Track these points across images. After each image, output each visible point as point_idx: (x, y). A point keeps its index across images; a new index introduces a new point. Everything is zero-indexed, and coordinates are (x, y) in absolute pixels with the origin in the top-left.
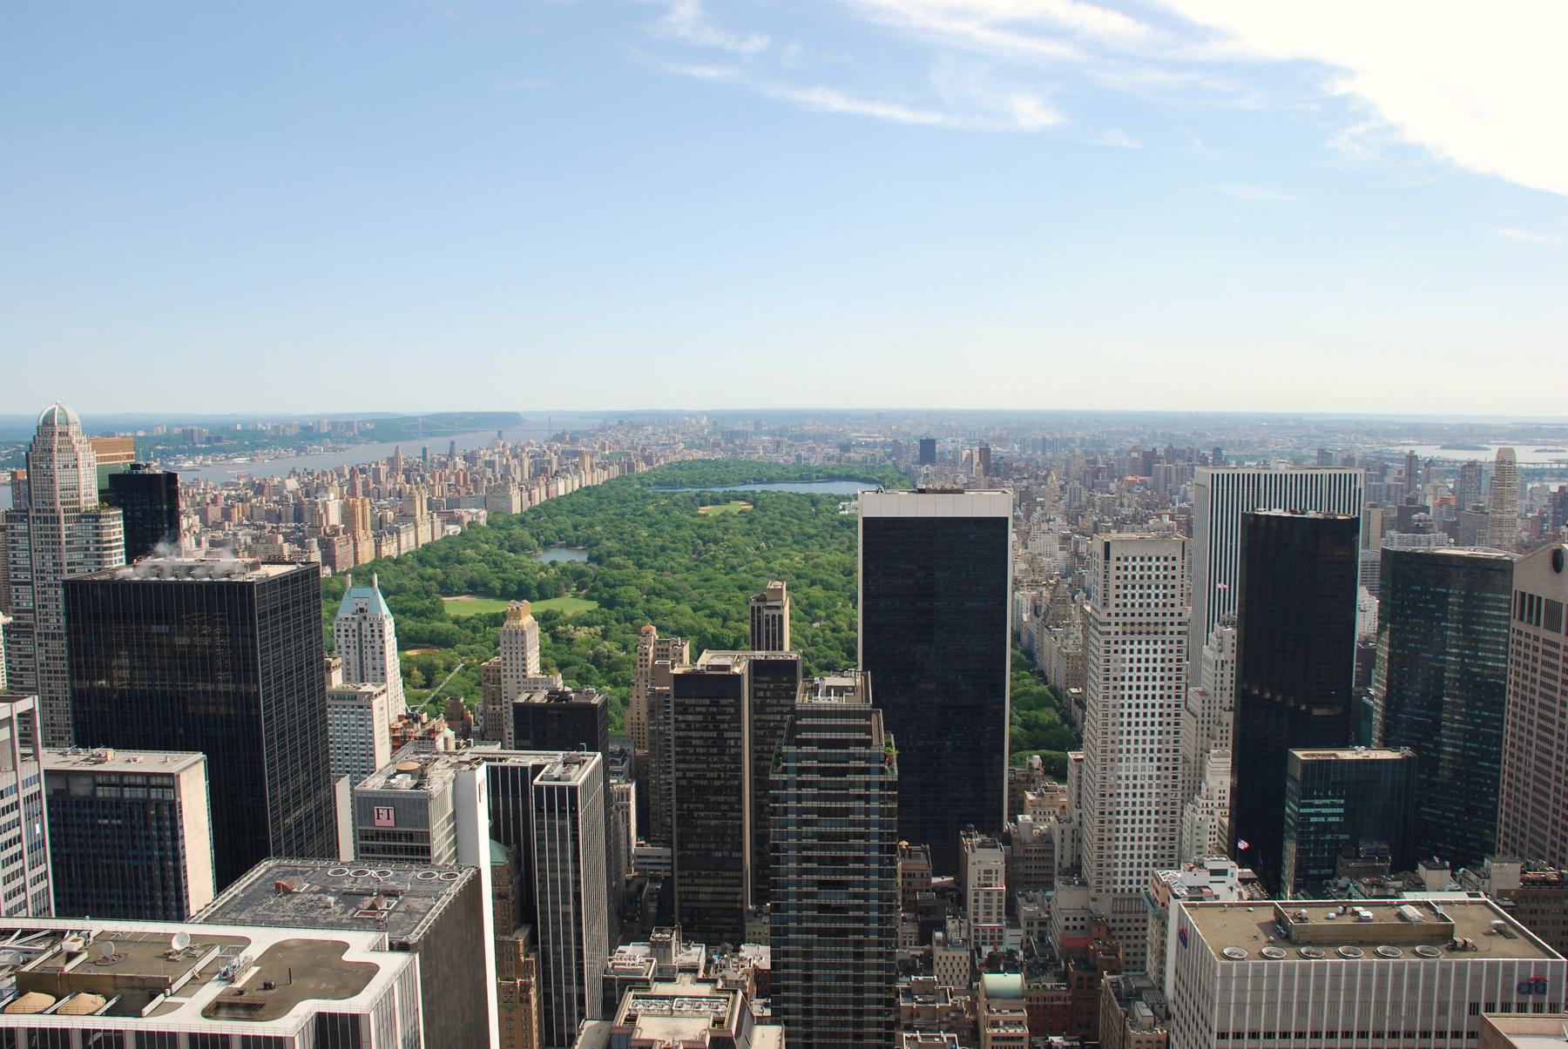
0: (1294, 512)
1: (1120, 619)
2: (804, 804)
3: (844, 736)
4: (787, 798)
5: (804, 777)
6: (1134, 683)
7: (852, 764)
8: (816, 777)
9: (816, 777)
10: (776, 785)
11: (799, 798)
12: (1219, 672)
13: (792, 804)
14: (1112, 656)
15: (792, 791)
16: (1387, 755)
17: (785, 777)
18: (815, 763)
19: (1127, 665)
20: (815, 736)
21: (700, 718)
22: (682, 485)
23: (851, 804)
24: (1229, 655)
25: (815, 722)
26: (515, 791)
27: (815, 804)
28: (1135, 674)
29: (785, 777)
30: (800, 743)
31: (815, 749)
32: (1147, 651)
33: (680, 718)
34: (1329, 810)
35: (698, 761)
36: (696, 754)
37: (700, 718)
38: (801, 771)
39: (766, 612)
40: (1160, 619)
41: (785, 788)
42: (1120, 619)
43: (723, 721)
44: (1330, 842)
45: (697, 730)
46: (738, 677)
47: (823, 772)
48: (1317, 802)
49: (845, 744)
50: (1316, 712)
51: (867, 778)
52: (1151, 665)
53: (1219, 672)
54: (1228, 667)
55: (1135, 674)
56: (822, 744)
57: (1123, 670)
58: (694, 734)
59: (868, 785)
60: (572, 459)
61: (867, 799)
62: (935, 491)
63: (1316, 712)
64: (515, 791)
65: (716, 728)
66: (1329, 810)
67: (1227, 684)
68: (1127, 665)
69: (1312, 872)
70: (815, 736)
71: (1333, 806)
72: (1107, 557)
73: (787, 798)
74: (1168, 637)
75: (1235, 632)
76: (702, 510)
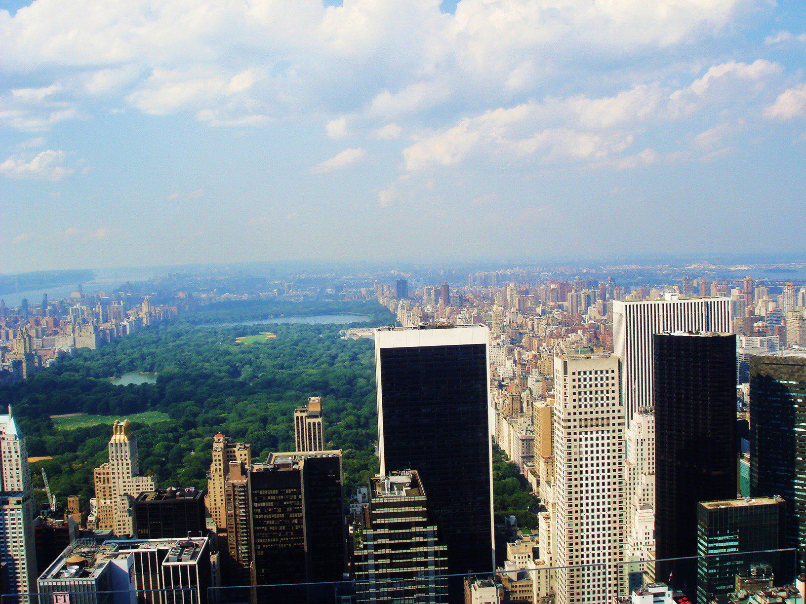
0: (691, 332)
1: (578, 417)
2: (381, 571)
3: (407, 520)
4: (367, 568)
5: (380, 552)
6: (589, 462)
7: (414, 540)
8: (388, 551)
9: (388, 551)
10: (359, 559)
11: (377, 567)
12: (640, 447)
13: (372, 571)
14: (573, 443)
15: (371, 562)
16: (756, 502)
17: (366, 552)
18: (387, 541)
19: (584, 449)
20: (387, 521)
21: (271, 504)
22: (222, 321)
23: (415, 569)
24: (650, 435)
25: (386, 510)
26: (146, 570)
27: (389, 571)
28: (589, 456)
29: (366, 552)
30: (376, 527)
31: (387, 531)
32: (597, 439)
33: (256, 505)
34: (727, 545)
35: (271, 537)
36: (269, 530)
37: (271, 504)
38: (377, 547)
39: (308, 420)
40: (605, 415)
41: (366, 560)
42: (578, 417)
43: (289, 506)
44: (730, 567)
45: (269, 513)
46: (297, 472)
47: (393, 547)
48: (720, 538)
49: (408, 525)
50: (714, 473)
51: (425, 549)
52: (600, 448)
53: (640, 447)
54: (645, 443)
55: (589, 456)
56: (392, 526)
57: (581, 453)
58: (267, 516)
59: (426, 555)
60: (133, 302)
61: (426, 564)
62: (432, 328)
63: (714, 473)
64: (146, 570)
65: (284, 511)
66: (727, 545)
67: (645, 456)
68: (584, 449)
69: (718, 588)
70: (387, 521)
71: (730, 540)
72: (565, 372)
73: (367, 568)
74: (611, 428)
75: (653, 418)
76: (239, 340)
